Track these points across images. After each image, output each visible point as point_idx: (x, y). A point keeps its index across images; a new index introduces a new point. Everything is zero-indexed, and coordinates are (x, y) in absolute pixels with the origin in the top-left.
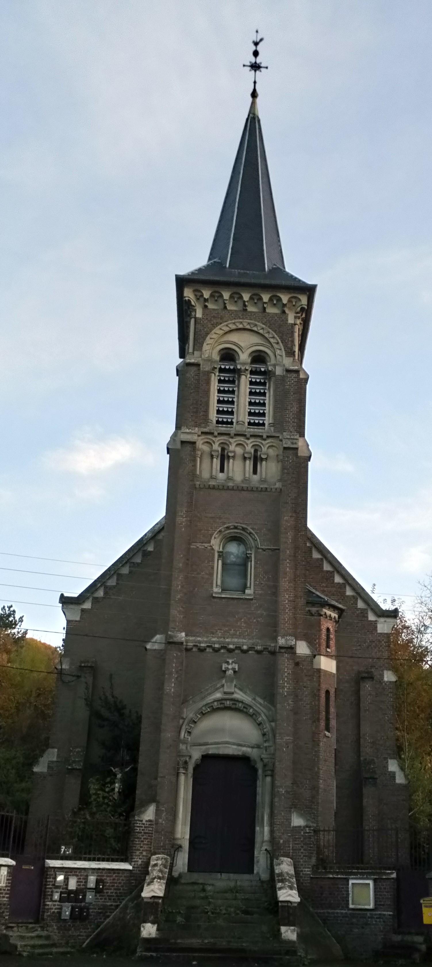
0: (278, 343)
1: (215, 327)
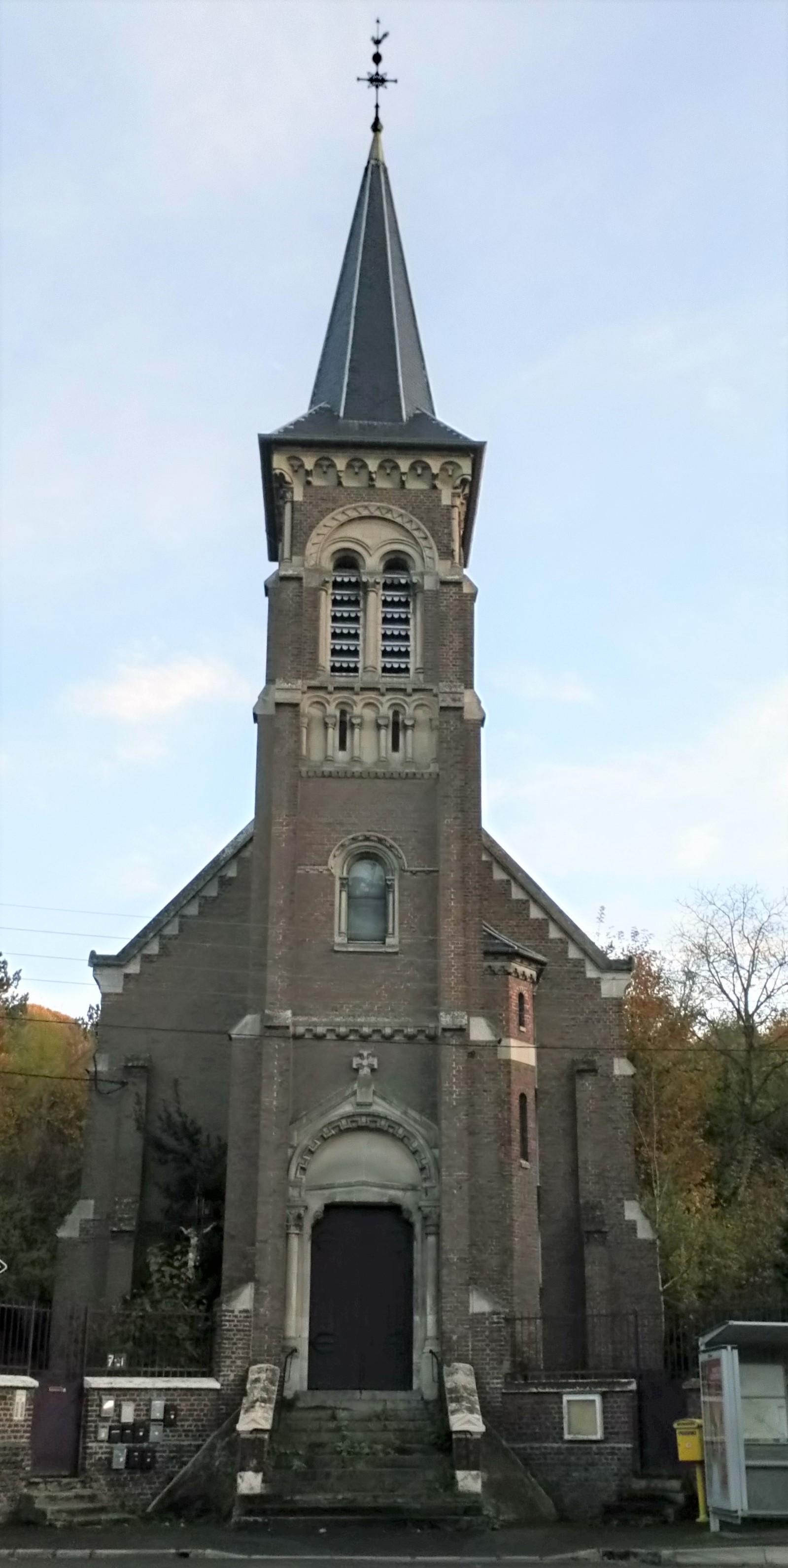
0: (426, 538)
1: (324, 517)
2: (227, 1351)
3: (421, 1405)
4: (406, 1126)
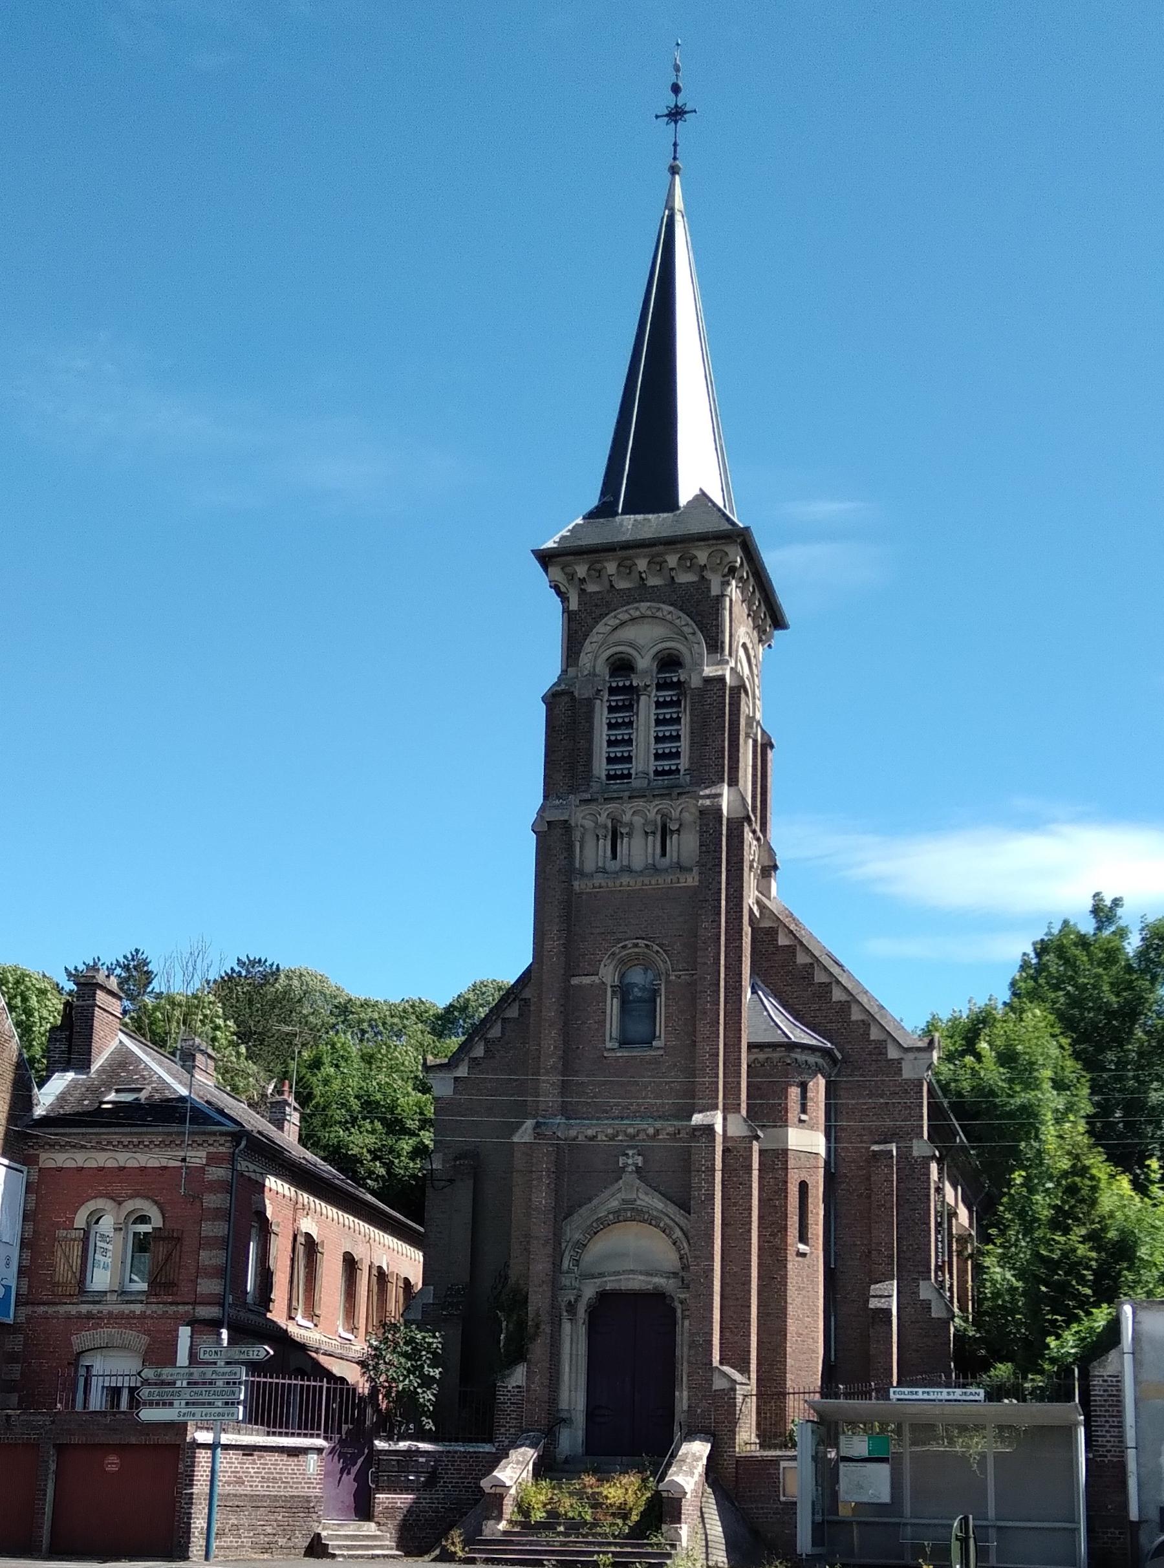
0: (694, 634)
1: (597, 623)
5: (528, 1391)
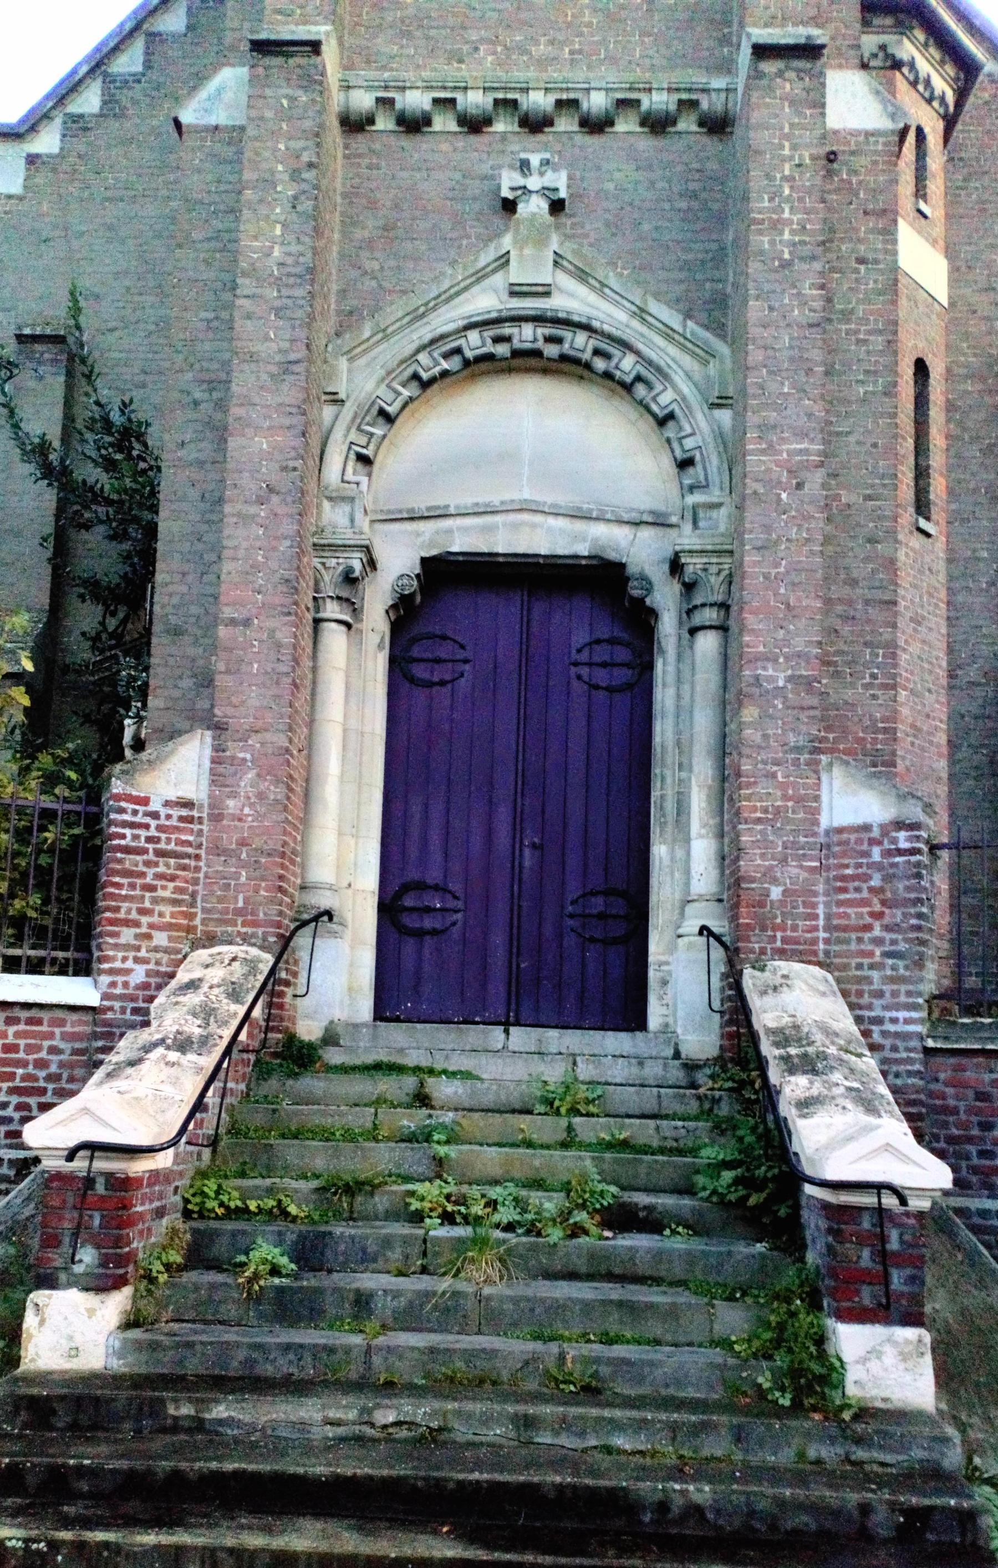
2: (125, 905)
3: (676, 1074)
4: (641, 347)
5: (216, 818)
